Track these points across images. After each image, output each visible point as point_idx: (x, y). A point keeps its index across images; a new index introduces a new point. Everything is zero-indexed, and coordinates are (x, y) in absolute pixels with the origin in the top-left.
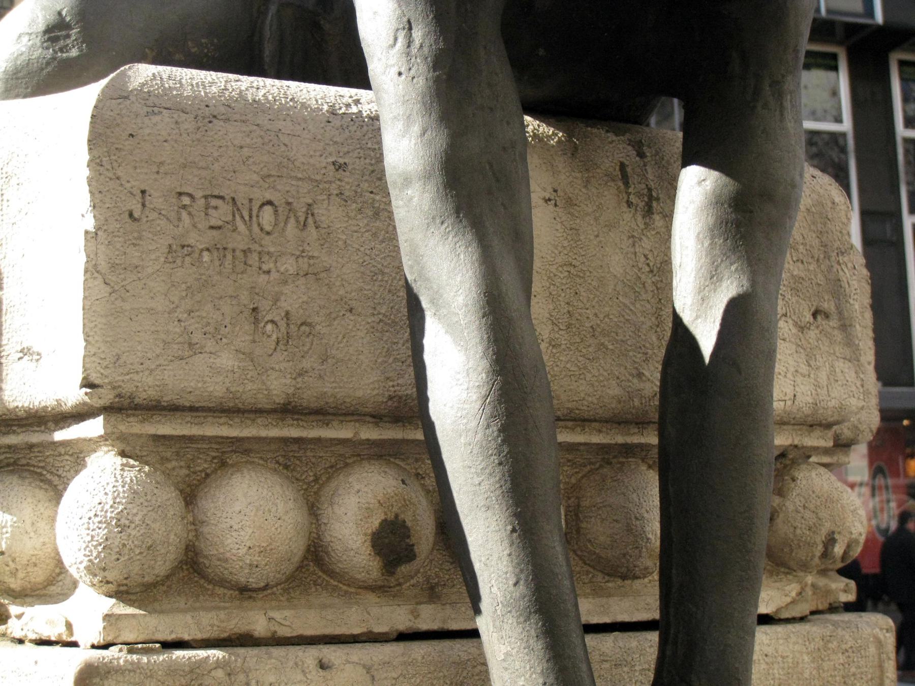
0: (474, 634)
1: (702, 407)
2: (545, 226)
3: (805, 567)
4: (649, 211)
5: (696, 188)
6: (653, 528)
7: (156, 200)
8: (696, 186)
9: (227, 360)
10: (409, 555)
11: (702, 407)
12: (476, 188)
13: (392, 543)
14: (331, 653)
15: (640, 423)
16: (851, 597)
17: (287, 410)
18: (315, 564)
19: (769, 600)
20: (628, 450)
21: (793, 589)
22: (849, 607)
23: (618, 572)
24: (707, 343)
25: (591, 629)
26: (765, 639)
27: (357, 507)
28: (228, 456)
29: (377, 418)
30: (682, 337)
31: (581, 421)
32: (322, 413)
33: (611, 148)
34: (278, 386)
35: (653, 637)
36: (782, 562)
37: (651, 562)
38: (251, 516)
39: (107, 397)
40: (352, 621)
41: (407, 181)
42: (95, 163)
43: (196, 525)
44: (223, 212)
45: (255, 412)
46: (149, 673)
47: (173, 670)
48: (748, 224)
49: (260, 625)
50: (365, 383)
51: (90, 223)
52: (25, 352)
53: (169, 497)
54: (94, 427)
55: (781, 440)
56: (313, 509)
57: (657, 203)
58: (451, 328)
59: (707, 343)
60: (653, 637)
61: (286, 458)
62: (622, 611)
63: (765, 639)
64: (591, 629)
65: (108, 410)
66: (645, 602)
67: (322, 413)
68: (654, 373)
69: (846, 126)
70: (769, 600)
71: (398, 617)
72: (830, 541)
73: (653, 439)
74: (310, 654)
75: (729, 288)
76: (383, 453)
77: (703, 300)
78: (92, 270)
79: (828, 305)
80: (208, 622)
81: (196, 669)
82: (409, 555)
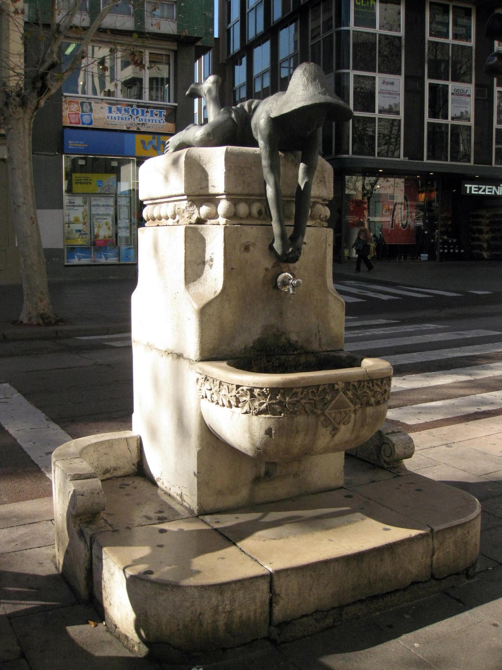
0: (271, 225)
1: (301, 197)
2: (282, 169)
3: (317, 219)
4: (296, 167)
5: (302, 166)
6: (294, 212)
7: (232, 167)
8: (302, 166)
9: (241, 188)
10: (262, 214)
11: (301, 197)
12: (274, 168)
13: (260, 212)
14: (253, 227)
15: (293, 197)
16: (327, 225)
17: (248, 195)
18: (250, 215)
19: (309, 223)
20: (291, 201)
21: (314, 222)
22: (326, 227)
23: (289, 218)
24: (302, 187)
25: (286, 226)
26: (308, 229)
27: (255, 208)
28: (241, 200)
29: (258, 196)
30: (299, 187)
31: (285, 197)
32: (251, 195)
33: (291, 157)
34: (246, 192)
35: (293, 228)
36: (313, 218)
37: (293, 217)
38: (243, 209)
39: (227, 193)
40: (254, 222)
41: (265, 167)
42: (225, 163)
43: (236, 209)
44: (240, 169)
45: (236, 195)
46: (232, 227)
47: (235, 227)
48: (309, 172)
49: (243, 222)
50: (257, 191)
51: (225, 171)
52: (213, 186)
53: (233, 206)
54: (224, 197)
55: (312, 200)
56: (250, 208)
57: (297, 166)
58: (270, 186)
59: (302, 187)
60: (293, 228)
61: (247, 201)
62: (289, 223)
63: (308, 229)
64: (286, 226)
65: (226, 195)
66: (292, 222)
67: (251, 195)
68: (295, 190)
69: (402, 33)
70: (309, 223)
71: (260, 222)
72: (320, 215)
73: (294, 199)
74: (250, 226)
75: (306, 181)
76: (259, 201)
77: (302, 182)
78: (225, 177)
79: (322, 180)
80: (238, 222)
81: (237, 227)
82: (262, 214)
